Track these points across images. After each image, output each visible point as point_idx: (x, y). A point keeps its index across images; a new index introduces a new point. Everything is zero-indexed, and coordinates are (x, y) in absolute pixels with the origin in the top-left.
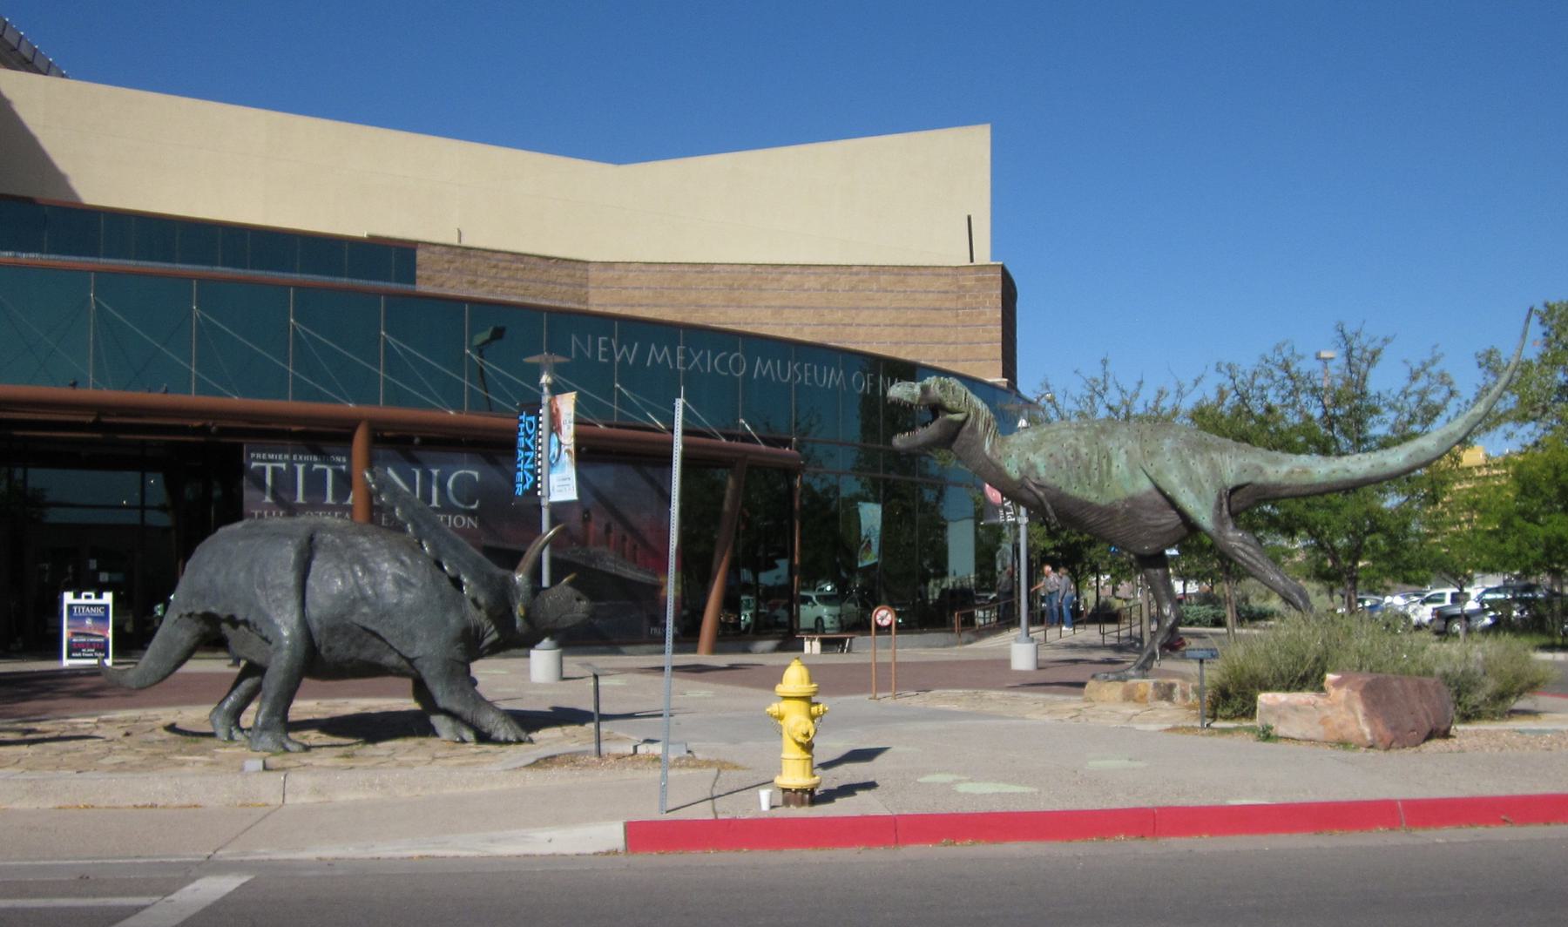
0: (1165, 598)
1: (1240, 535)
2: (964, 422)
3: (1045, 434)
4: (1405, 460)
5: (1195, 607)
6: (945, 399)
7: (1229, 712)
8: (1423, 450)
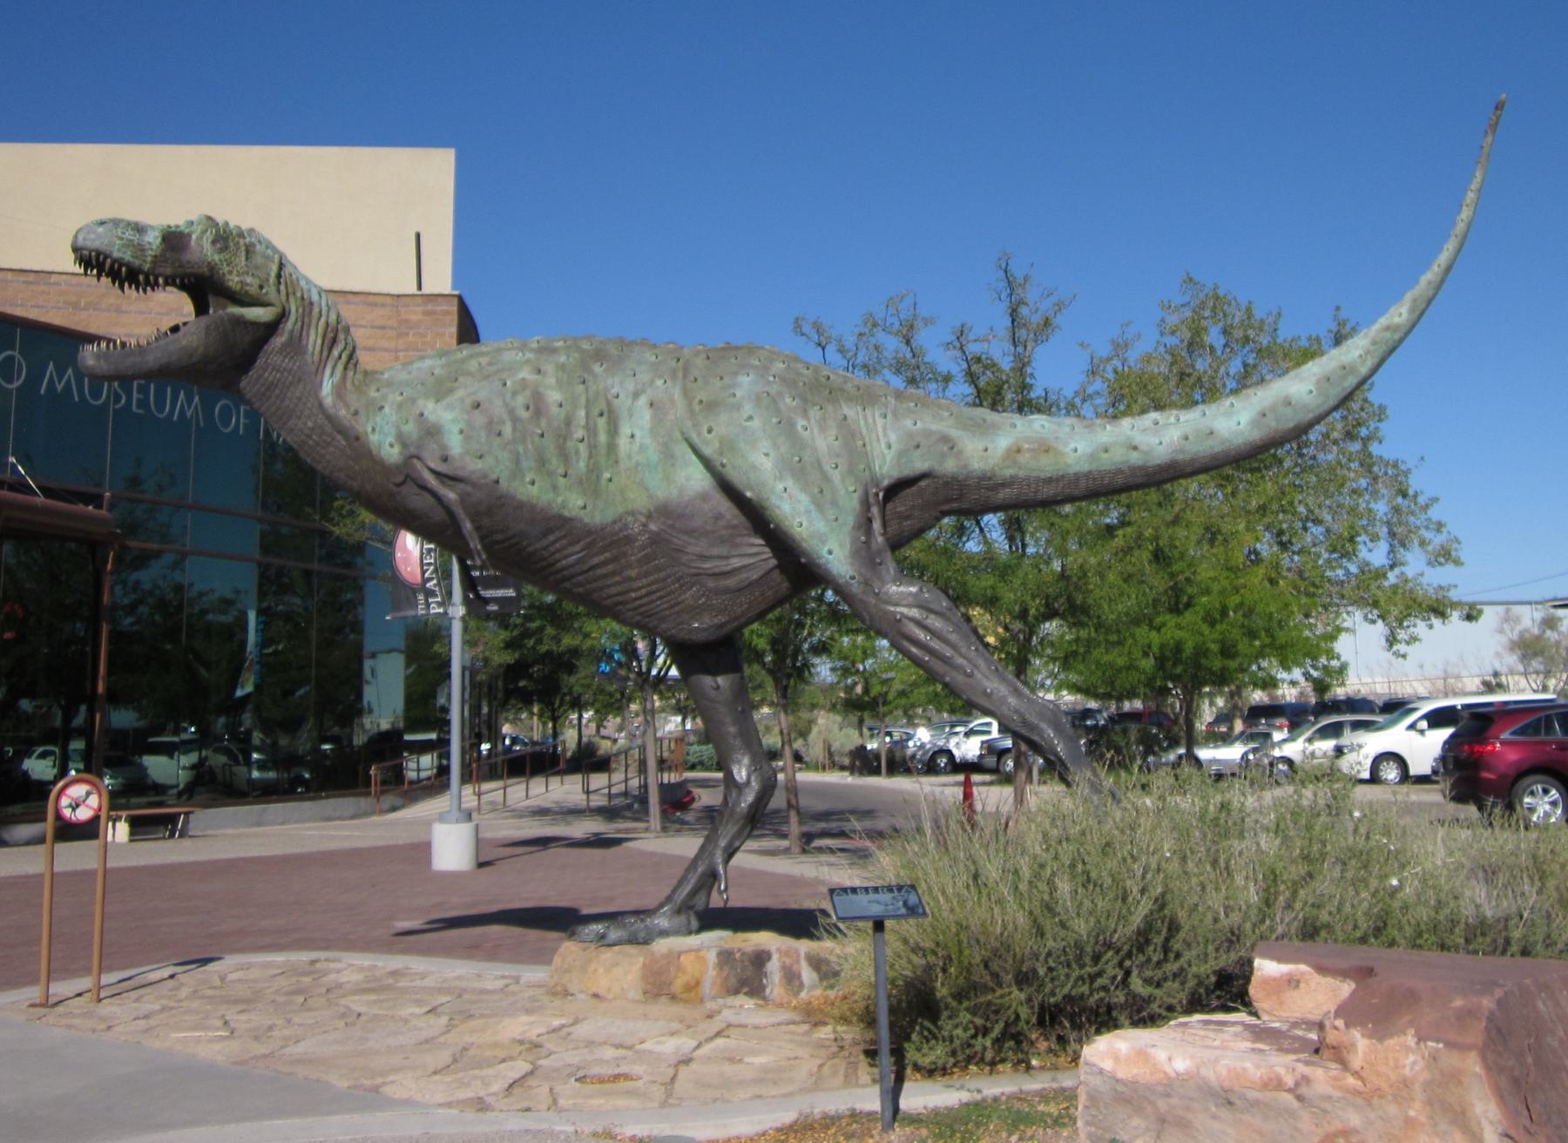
0: (738, 742)
1: (913, 589)
2: (272, 328)
3: (463, 361)
4: (1254, 423)
5: (695, 748)
6: (226, 269)
7: (937, 1053)
8: (1288, 402)
